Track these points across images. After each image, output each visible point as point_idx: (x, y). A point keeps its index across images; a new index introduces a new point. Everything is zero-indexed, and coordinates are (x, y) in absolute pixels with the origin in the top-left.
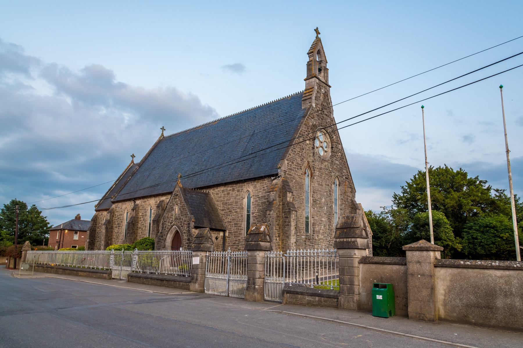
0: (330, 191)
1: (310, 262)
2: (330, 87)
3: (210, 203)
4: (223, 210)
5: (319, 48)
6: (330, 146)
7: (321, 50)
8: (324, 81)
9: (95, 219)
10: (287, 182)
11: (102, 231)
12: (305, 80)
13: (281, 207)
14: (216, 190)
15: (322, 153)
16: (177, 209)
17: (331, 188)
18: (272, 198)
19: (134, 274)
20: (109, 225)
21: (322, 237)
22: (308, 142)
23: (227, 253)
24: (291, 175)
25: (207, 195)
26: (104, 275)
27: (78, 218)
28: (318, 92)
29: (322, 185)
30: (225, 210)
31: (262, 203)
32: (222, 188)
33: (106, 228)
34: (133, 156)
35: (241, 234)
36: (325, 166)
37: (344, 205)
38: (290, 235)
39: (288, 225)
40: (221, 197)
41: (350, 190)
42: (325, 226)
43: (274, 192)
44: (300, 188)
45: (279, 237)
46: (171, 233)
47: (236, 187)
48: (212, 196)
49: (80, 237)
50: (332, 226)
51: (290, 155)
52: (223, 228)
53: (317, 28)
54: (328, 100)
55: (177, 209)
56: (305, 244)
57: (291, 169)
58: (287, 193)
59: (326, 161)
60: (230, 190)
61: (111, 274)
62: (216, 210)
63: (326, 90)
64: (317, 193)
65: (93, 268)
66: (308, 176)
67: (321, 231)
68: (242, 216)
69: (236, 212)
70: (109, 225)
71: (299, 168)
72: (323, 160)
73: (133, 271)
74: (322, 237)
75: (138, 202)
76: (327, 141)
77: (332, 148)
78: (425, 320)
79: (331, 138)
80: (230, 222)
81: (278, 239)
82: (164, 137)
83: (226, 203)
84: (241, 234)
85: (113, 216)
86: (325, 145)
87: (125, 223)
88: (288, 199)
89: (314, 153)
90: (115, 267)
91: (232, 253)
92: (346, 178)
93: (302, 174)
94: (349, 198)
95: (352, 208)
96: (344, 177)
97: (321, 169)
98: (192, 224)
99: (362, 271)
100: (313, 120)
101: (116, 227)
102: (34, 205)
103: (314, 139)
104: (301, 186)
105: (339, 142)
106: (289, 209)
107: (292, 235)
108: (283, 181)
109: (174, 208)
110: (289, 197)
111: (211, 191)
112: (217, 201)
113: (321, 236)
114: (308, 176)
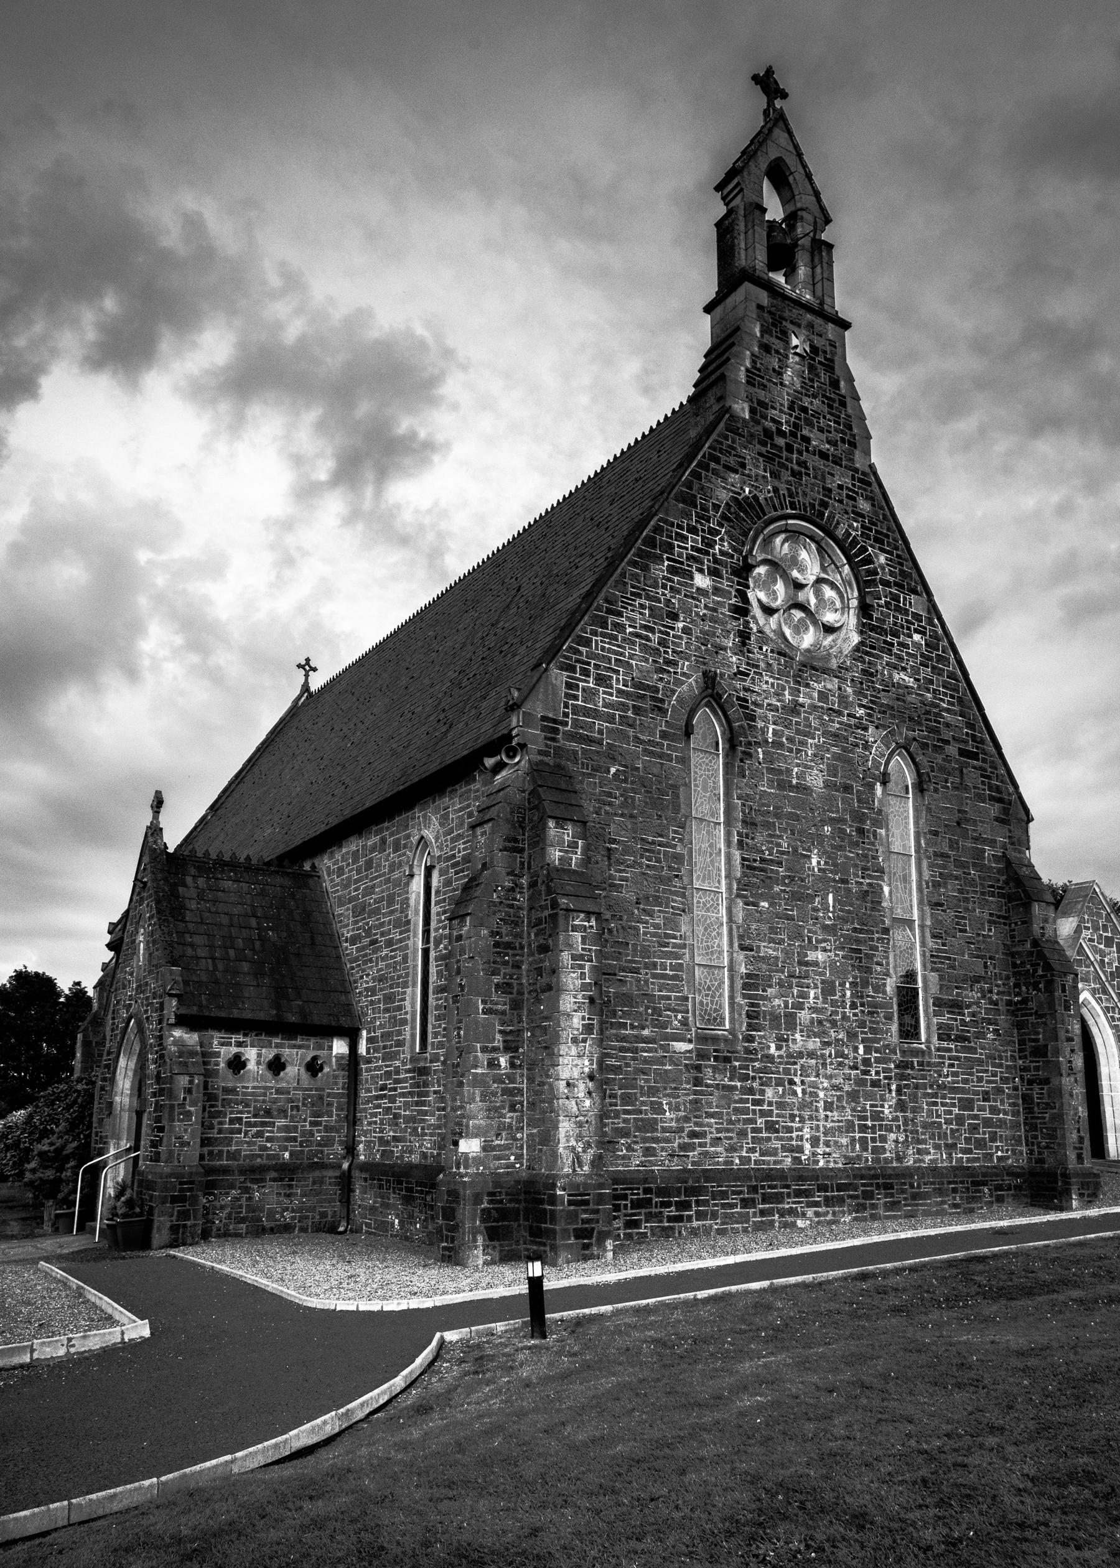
0: (859, 818)
2: (845, 325)
3: (307, 915)
5: (773, 153)
6: (854, 603)
7: (791, 161)
8: (815, 303)
10: (559, 770)
12: (708, 309)
13: (522, 899)
21: (814, 1044)
22: (701, 581)
24: (590, 740)
28: (766, 348)
35: (400, 1044)
36: (823, 696)
37: (952, 884)
38: (556, 1039)
39: (549, 988)
41: (994, 810)
42: (828, 989)
43: (487, 827)
44: (656, 803)
45: (510, 1047)
46: (129, 1055)
47: (389, 831)
48: (327, 885)
50: (880, 988)
52: (345, 1022)
53: (769, 71)
54: (835, 384)
56: (698, 1082)
58: (545, 827)
59: (825, 671)
60: (373, 849)
62: (333, 940)
63: (819, 342)
64: (768, 825)
67: (804, 1016)
71: (647, 705)
74: (814, 1044)
76: (837, 579)
79: (859, 563)
81: (503, 1061)
82: (311, 695)
84: (400, 1044)
88: (555, 855)
89: (744, 636)
92: (963, 753)
93: (664, 735)
94: (988, 851)
95: (1010, 898)
96: (952, 750)
97: (794, 708)
99: (1021, 1215)
100: (734, 478)
102: (79, 984)
105: (911, 578)
106: (555, 905)
107: (566, 1035)
108: (536, 770)
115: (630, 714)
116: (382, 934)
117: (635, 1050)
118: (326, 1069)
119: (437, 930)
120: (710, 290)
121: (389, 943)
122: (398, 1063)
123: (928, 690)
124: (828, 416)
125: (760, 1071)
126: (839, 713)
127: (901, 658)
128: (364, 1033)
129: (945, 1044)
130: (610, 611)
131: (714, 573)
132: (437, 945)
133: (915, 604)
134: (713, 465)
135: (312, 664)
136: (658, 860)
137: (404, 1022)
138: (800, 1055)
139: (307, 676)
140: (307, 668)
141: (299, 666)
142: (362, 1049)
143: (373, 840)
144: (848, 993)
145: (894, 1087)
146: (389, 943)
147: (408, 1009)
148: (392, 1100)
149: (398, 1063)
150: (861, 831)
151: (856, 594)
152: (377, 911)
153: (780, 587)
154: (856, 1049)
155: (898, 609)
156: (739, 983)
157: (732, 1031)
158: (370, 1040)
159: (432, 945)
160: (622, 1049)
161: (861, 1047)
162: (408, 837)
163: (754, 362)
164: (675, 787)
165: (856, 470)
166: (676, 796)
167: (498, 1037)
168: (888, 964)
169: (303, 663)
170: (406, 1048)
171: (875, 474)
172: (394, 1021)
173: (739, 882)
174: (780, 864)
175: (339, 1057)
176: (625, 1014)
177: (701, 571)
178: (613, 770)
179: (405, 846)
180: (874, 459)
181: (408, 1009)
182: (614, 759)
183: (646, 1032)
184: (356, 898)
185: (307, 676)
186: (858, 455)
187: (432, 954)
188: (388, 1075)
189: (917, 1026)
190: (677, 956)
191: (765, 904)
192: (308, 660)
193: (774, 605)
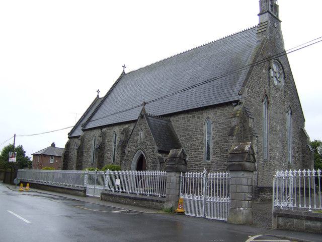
1: (219, 185)
2: (281, 22)
4: (183, 136)
9: (68, 145)
11: (74, 155)
12: (259, 15)
14: (177, 117)
15: (276, 83)
16: (142, 134)
17: (285, 116)
18: (233, 124)
19: (107, 192)
20: (80, 150)
23: (202, 173)
25: (169, 121)
26: (80, 192)
27: (53, 145)
29: (277, 113)
30: (185, 136)
31: (223, 129)
32: (182, 116)
33: (78, 152)
34: (98, 91)
40: (181, 124)
47: (196, 114)
49: (55, 161)
51: (249, 82)
55: (142, 134)
57: (251, 97)
61: (85, 191)
65: (69, 186)
66: (265, 104)
67: (277, 157)
68: (202, 141)
69: (197, 138)
70: (80, 150)
72: (277, 89)
73: (106, 190)
75: (104, 130)
77: (285, 77)
78: (293, 231)
80: (191, 147)
83: (187, 130)
85: (83, 142)
86: (278, 75)
87: (93, 148)
90: (89, 186)
91: (209, 174)
98: (156, 149)
101: (86, 152)
103: (270, 69)
104: (260, 115)
109: (139, 133)
110: (251, 123)
111: (172, 119)
112: (178, 127)
113: (277, 163)
114: (265, 104)
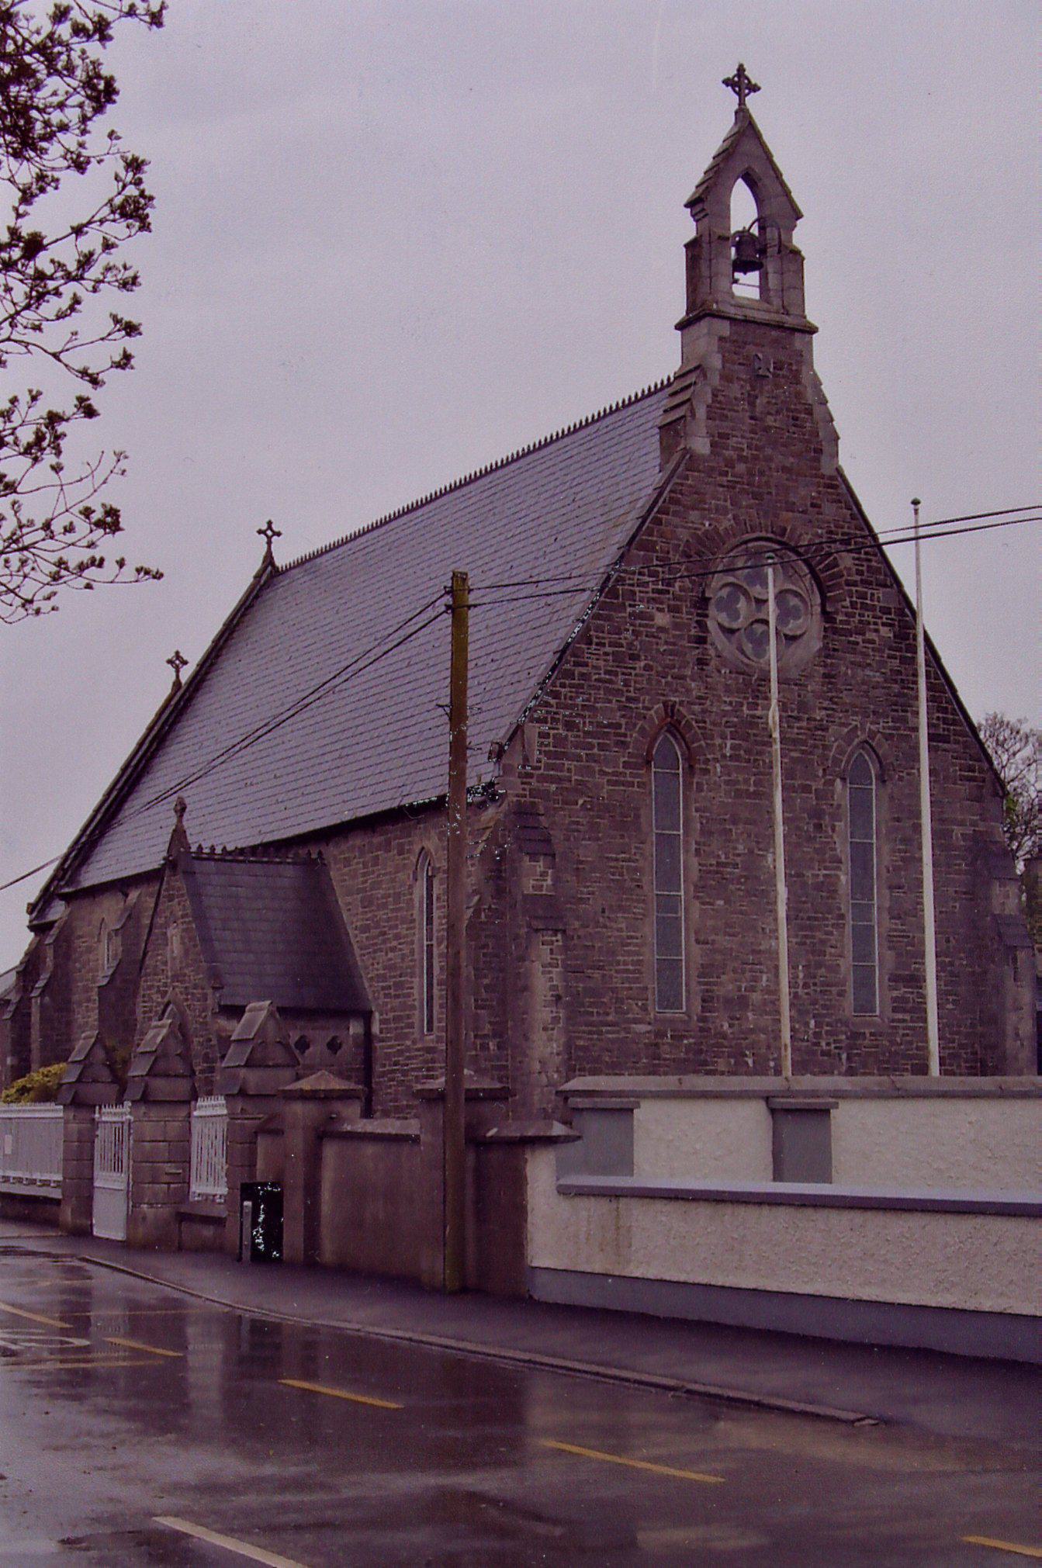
53: (741, 70)
94: (958, 831)
100: (694, 515)
115: (596, 751)
116: (391, 928)
117: (600, 1033)
118: (344, 1046)
119: (438, 931)
120: (680, 312)
121: (397, 937)
122: (408, 1043)
123: (895, 681)
124: (793, 429)
125: (713, 1045)
126: (798, 719)
127: (866, 655)
128: (377, 1015)
129: (900, 1016)
130: (577, 664)
131: (674, 610)
132: (439, 944)
133: (881, 596)
134: (673, 508)
135: (275, 528)
136: (621, 874)
137: (413, 1007)
138: (752, 1031)
139: (269, 543)
140: (269, 533)
141: (260, 532)
142: (376, 1028)
143: (377, 840)
144: (801, 975)
145: (844, 1056)
146: (397, 937)
147: (416, 996)
148: (405, 1073)
149: (408, 1043)
150: (819, 827)
151: (819, 601)
152: (385, 906)
153: (742, 604)
154: (807, 1024)
155: (864, 607)
156: (694, 973)
157: (687, 1014)
158: (382, 1022)
159: (434, 942)
160: (590, 1033)
161: (812, 1022)
162: (411, 843)
163: (715, 395)
164: (637, 809)
165: (823, 477)
166: (637, 817)
167: (488, 1026)
168: (843, 947)
169: (265, 527)
170: (416, 1030)
171: (842, 476)
172: (404, 1007)
173: (696, 886)
174: (735, 866)
175: (356, 1037)
176: (592, 1005)
177: (660, 610)
178: (581, 802)
179: (409, 851)
180: (840, 463)
181: (416, 996)
182: (582, 794)
183: (610, 1018)
184: (364, 890)
185: (269, 543)
186: (824, 459)
187: (435, 951)
188: (400, 1053)
189: (872, 1001)
190: (638, 954)
191: (721, 902)
192: (270, 523)
193: (735, 626)
